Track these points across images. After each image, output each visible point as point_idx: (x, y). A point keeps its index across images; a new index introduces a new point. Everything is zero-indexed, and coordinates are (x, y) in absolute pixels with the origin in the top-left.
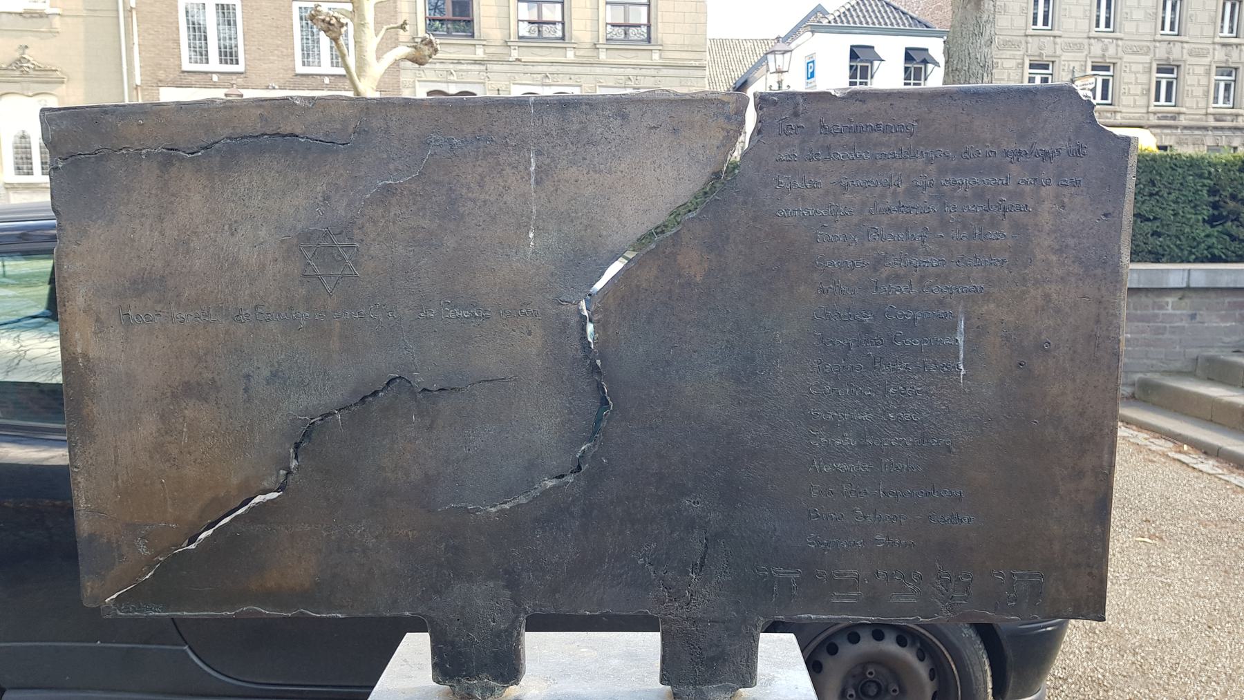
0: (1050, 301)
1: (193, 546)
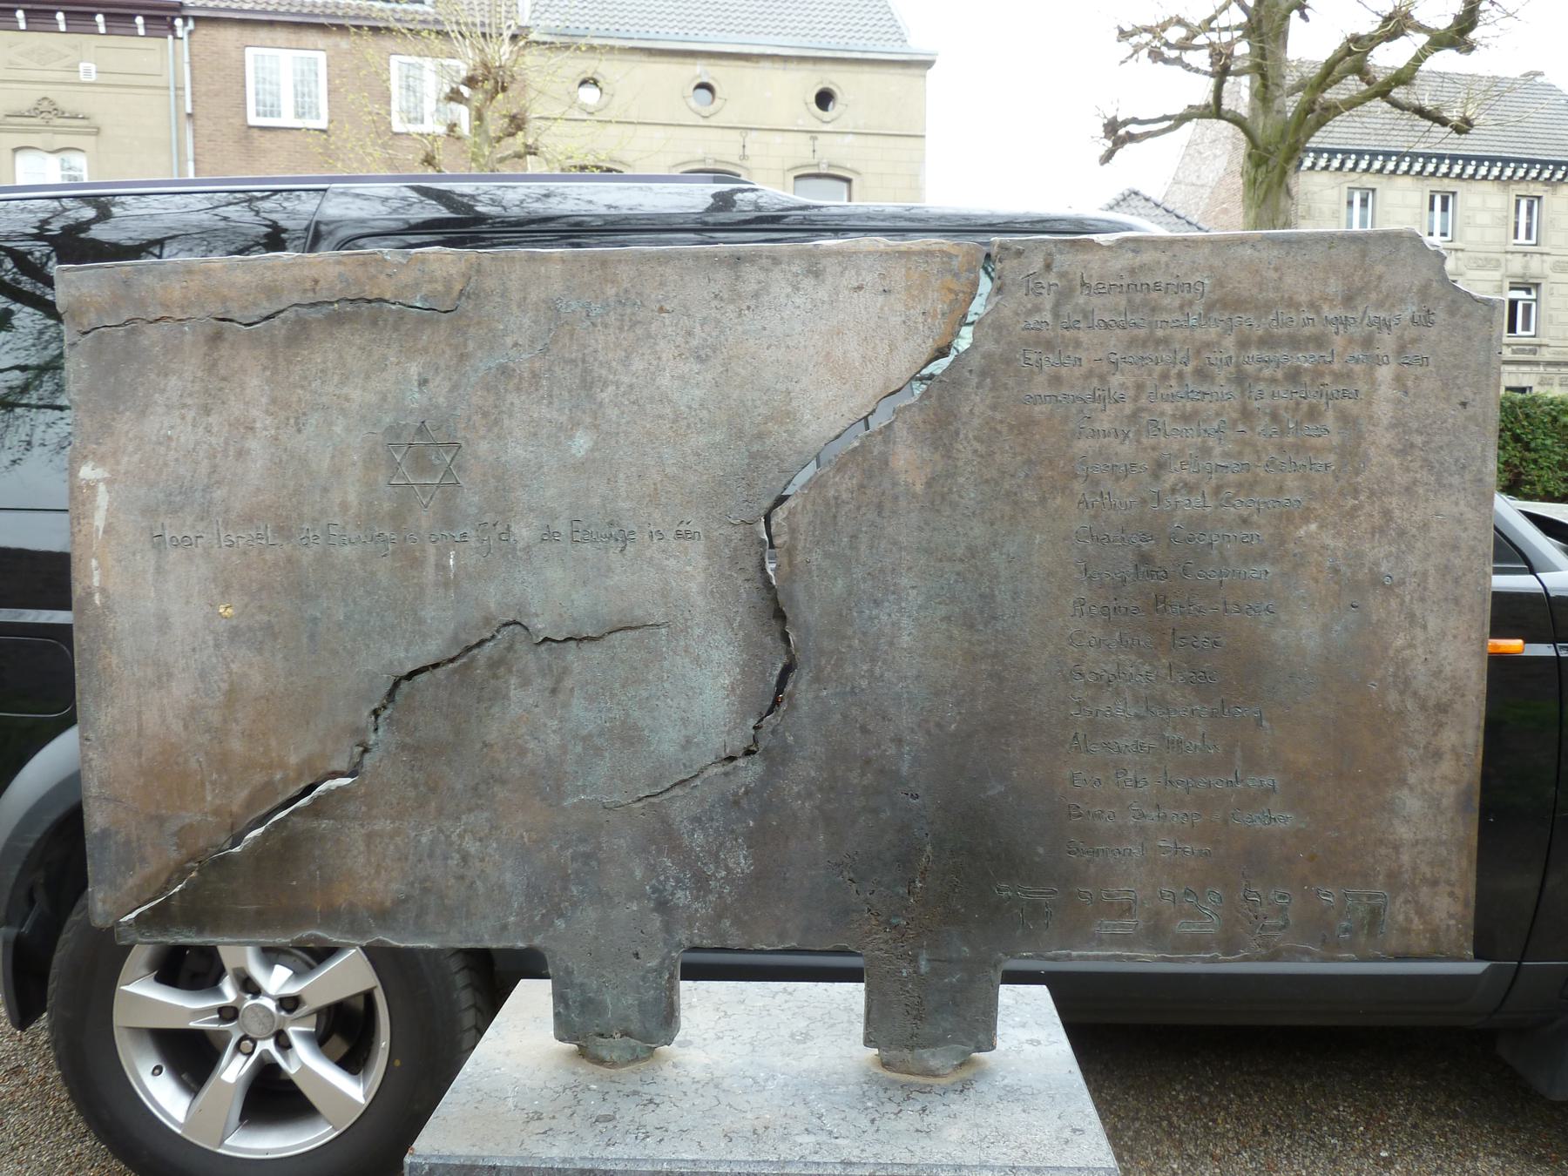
0: (1391, 519)
1: (237, 849)
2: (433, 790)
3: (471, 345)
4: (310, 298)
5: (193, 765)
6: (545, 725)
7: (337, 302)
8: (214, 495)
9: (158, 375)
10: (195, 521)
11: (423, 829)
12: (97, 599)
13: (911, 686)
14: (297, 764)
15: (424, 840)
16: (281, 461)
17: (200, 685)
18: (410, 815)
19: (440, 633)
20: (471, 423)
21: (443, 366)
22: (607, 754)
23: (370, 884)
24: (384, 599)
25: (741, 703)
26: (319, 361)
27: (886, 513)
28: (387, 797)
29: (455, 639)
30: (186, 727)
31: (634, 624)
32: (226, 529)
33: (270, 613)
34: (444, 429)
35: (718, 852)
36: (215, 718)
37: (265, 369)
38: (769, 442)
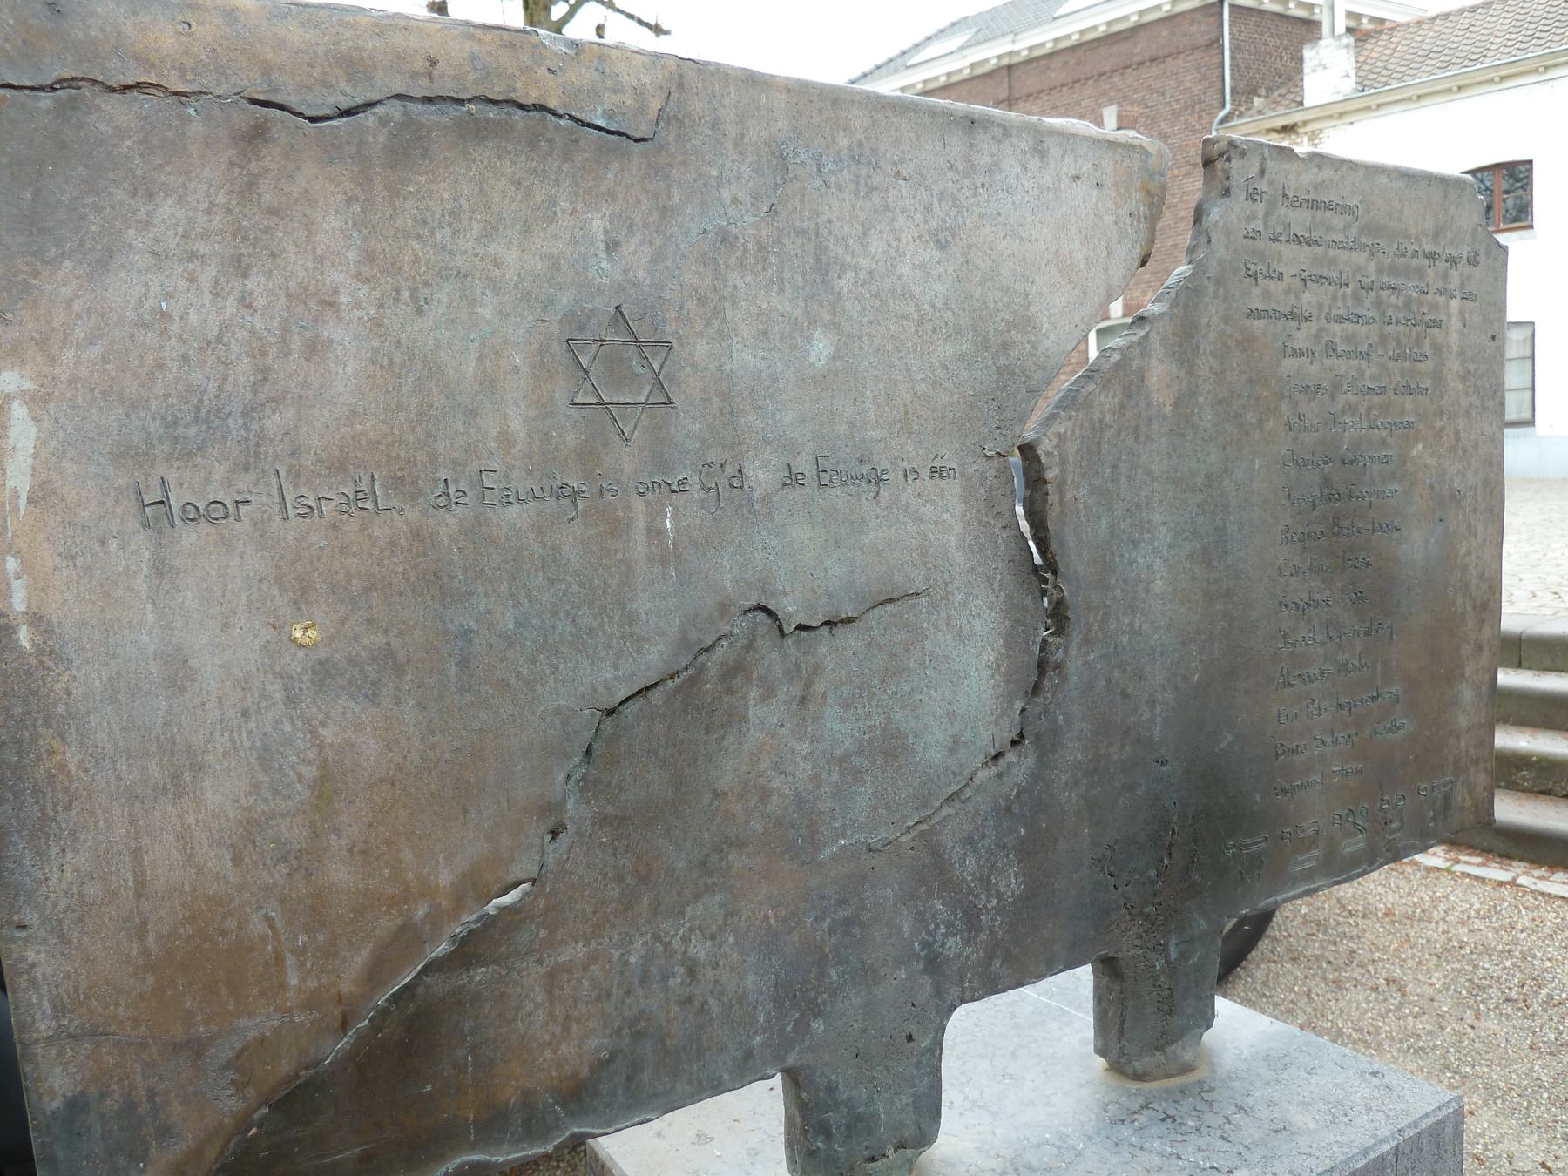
2: (644, 879)
3: (676, 195)
4: (421, 88)
5: (257, 926)
6: (793, 751)
7: (469, 101)
8: (268, 424)
9: (134, 194)
10: (233, 471)
11: (631, 943)
12: (24, 637)
13: (1164, 637)
14: (452, 884)
15: (633, 959)
16: (391, 362)
17: (261, 776)
18: (613, 926)
19: (662, 634)
20: (685, 312)
21: (638, 220)
22: (868, 778)
23: (554, 1051)
24: (575, 588)
25: (1007, 682)
26: (446, 195)
27: (1142, 439)
28: (578, 907)
29: (684, 640)
30: (237, 860)
31: (895, 596)
32: (296, 486)
33: (386, 631)
34: (648, 319)
35: (989, 877)
36: (295, 834)
37: (350, 200)
38: (1014, 353)
